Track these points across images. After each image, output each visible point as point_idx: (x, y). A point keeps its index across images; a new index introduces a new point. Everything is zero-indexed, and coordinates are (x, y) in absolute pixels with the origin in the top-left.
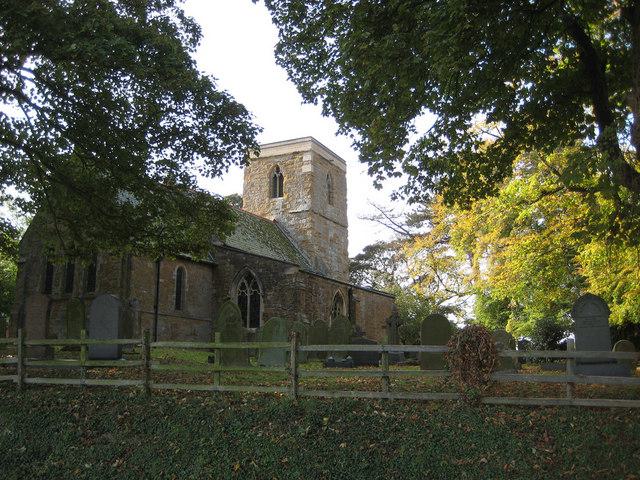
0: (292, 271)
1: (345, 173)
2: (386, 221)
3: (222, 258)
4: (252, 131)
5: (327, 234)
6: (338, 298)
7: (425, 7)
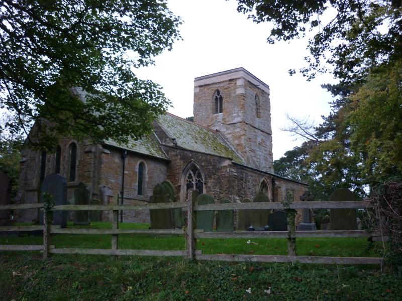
0: (227, 163)
1: (269, 95)
2: (301, 131)
4: (329, 90)
5: (256, 139)
6: (264, 185)
7: (36, 171)
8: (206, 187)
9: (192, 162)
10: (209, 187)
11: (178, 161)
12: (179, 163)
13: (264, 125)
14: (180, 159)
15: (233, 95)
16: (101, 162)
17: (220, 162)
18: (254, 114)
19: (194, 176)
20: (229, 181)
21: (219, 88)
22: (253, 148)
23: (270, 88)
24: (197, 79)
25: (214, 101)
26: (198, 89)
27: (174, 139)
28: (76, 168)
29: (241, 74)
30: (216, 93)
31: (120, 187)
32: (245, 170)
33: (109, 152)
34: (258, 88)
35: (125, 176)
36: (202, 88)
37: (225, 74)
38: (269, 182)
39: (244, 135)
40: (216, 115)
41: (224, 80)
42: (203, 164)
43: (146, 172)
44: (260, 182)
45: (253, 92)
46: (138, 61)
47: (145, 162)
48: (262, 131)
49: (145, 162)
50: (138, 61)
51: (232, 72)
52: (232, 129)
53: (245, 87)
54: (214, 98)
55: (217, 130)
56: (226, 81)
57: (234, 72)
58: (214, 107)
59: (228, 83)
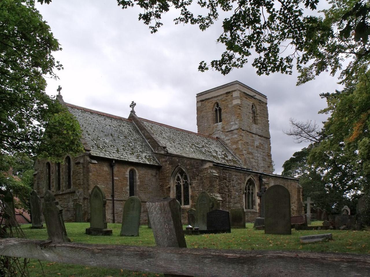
0: (207, 165)
1: (266, 104)
3: (164, 162)
7: (45, 182)
8: (191, 188)
9: (179, 166)
10: (194, 187)
11: (168, 166)
12: (168, 167)
13: (262, 130)
14: (169, 164)
15: (230, 106)
16: (88, 171)
17: (202, 165)
18: (251, 121)
19: (182, 178)
20: (210, 182)
21: (218, 101)
22: (250, 151)
23: (267, 98)
24: (199, 95)
25: (214, 113)
26: (200, 103)
27: (165, 148)
28: (71, 178)
29: (237, 87)
30: (216, 105)
31: (111, 191)
32: (228, 170)
33: (96, 162)
34: (255, 98)
35: (115, 182)
36: (203, 102)
37: (223, 88)
38: (256, 180)
39: (241, 140)
40: (216, 124)
41: (222, 93)
42: (188, 167)
43: (137, 177)
44: (245, 180)
45: (250, 102)
46: (250, 54)
47: (135, 169)
48: (260, 136)
49: (135, 169)
50: (250, 54)
51: (228, 86)
52: (230, 135)
53: (240, 98)
54: (214, 110)
55: (217, 137)
56: (224, 94)
57: (230, 85)
58: (214, 117)
59: (225, 95)
